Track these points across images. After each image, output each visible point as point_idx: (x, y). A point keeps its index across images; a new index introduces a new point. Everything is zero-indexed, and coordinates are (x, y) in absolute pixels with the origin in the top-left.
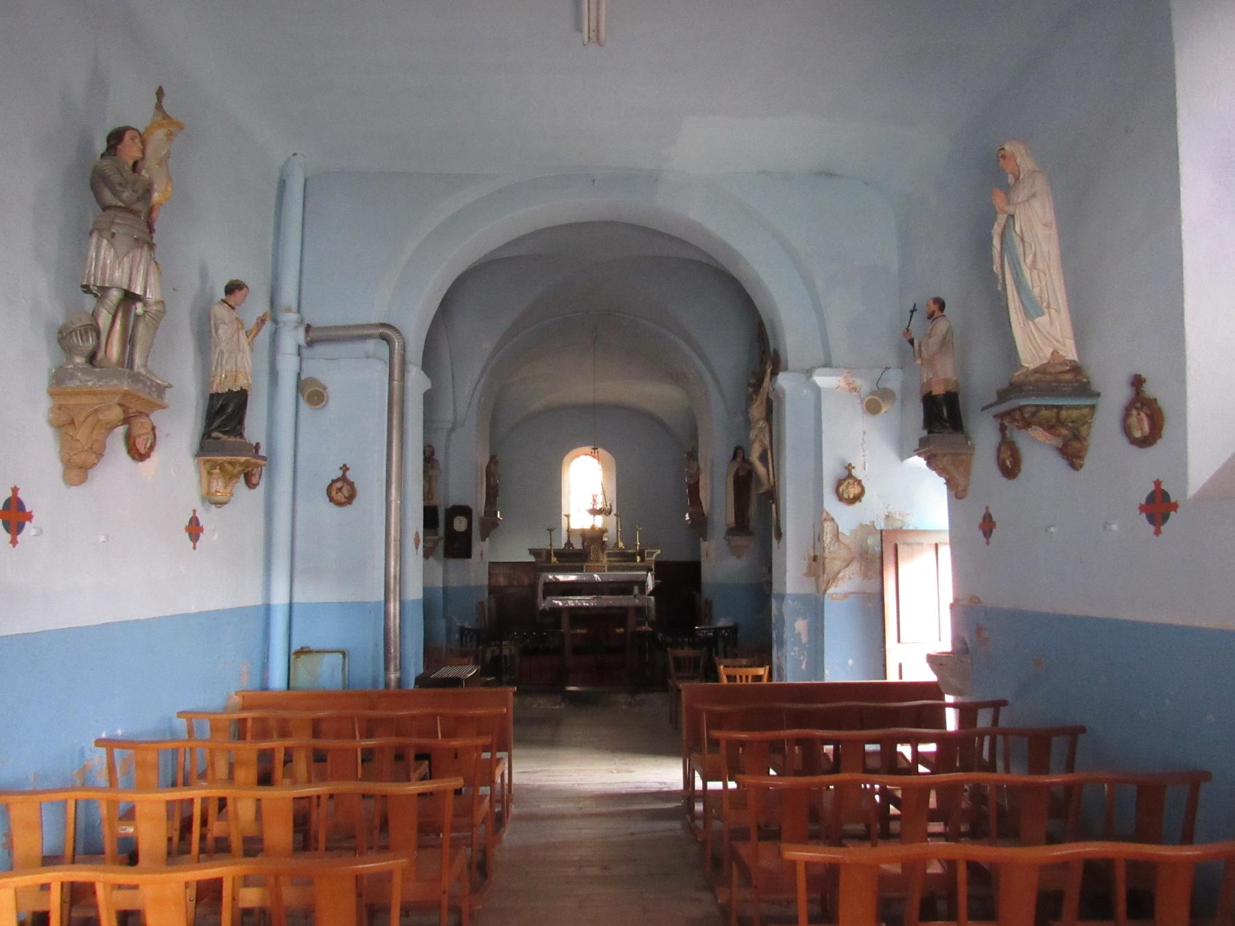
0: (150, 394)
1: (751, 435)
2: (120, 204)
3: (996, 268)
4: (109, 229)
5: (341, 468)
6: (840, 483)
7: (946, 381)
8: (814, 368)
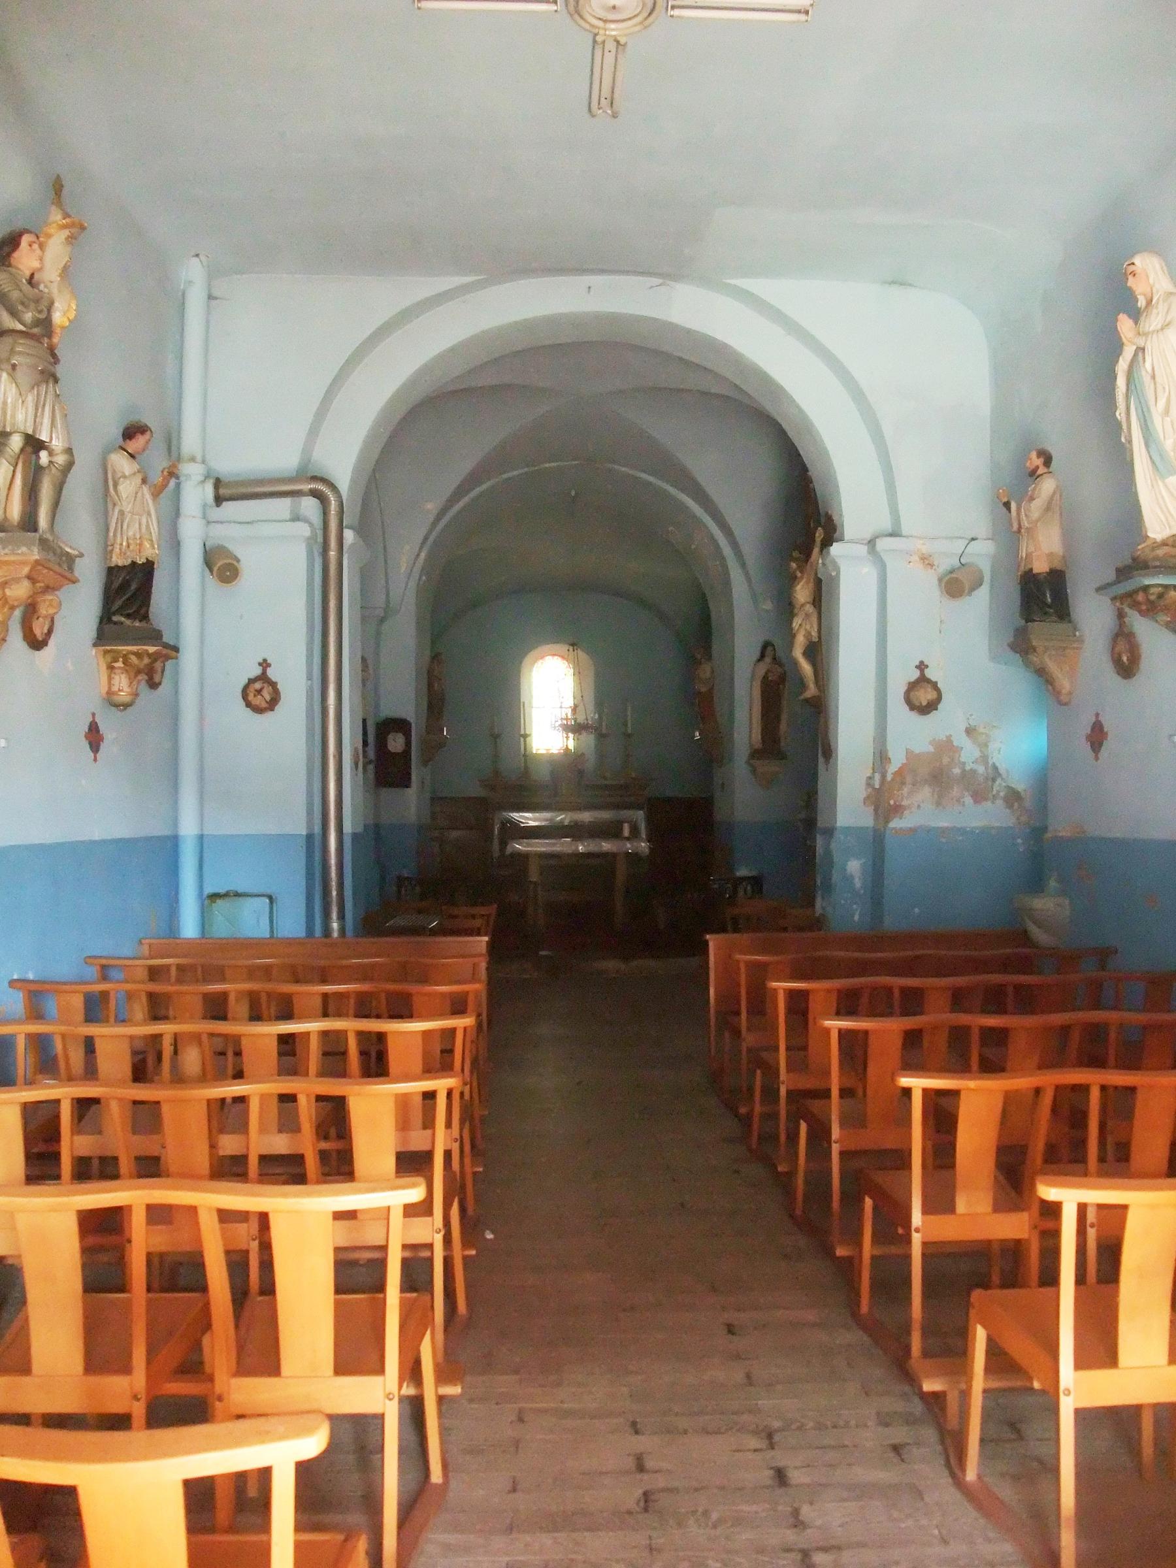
0: (60, 565)
1: (794, 624)
2: (20, 327)
3: (1120, 414)
4: (8, 360)
5: (260, 664)
6: (912, 686)
7: (1051, 555)
8: (877, 537)
